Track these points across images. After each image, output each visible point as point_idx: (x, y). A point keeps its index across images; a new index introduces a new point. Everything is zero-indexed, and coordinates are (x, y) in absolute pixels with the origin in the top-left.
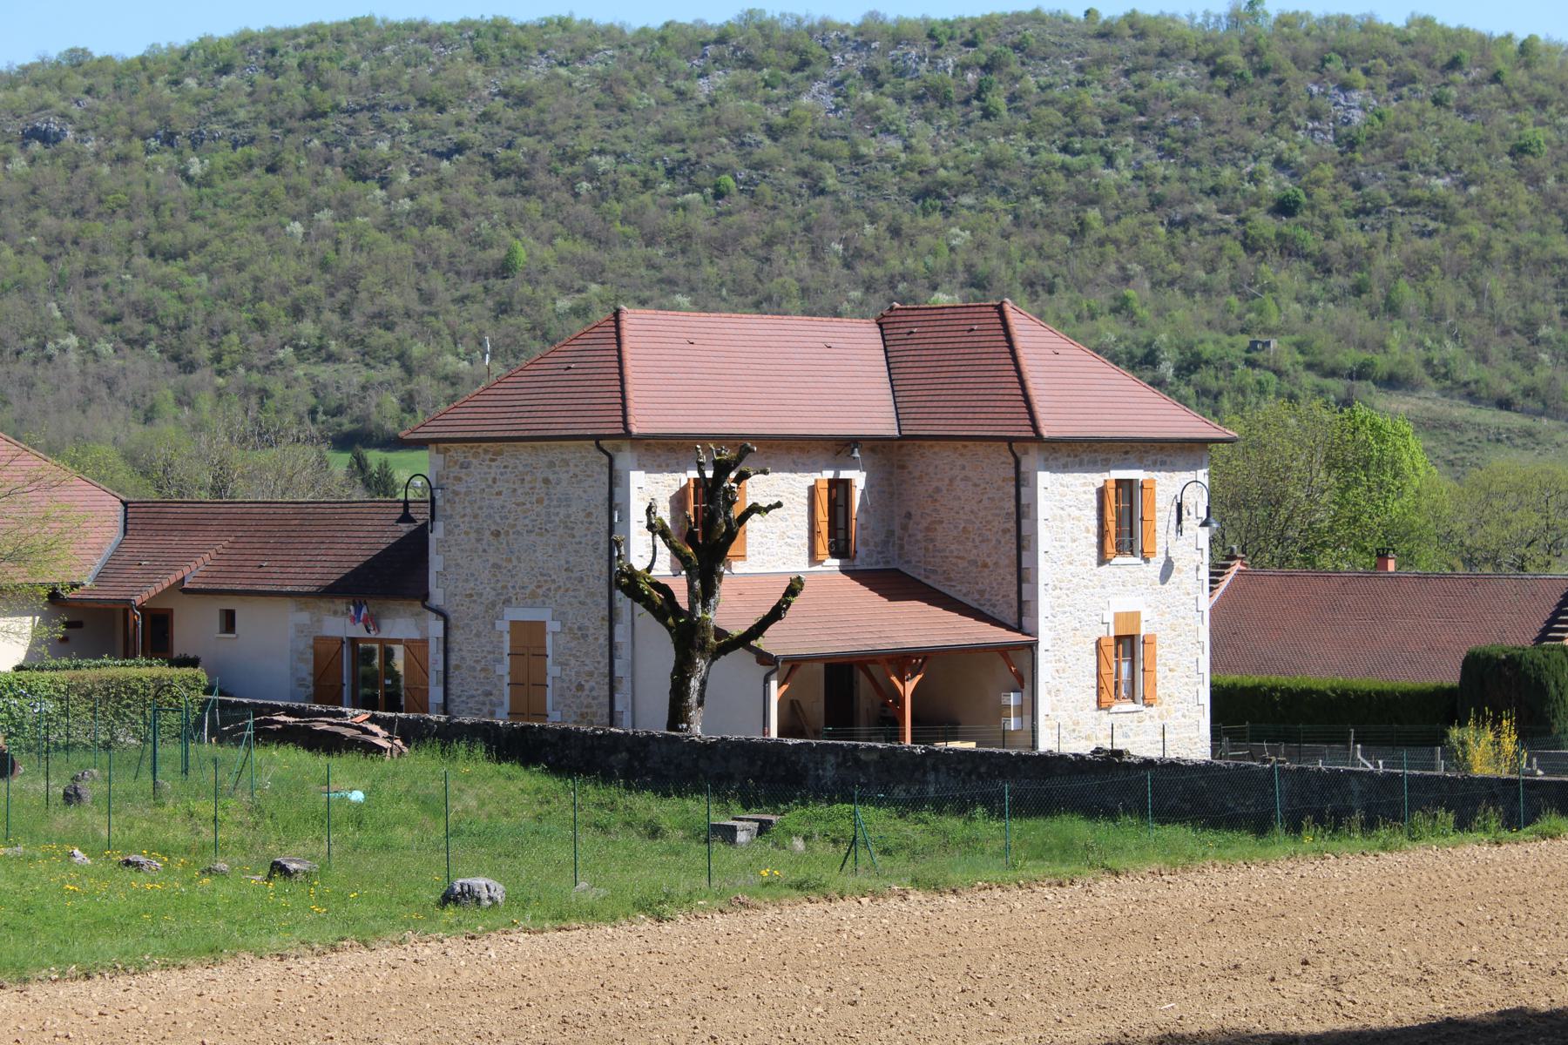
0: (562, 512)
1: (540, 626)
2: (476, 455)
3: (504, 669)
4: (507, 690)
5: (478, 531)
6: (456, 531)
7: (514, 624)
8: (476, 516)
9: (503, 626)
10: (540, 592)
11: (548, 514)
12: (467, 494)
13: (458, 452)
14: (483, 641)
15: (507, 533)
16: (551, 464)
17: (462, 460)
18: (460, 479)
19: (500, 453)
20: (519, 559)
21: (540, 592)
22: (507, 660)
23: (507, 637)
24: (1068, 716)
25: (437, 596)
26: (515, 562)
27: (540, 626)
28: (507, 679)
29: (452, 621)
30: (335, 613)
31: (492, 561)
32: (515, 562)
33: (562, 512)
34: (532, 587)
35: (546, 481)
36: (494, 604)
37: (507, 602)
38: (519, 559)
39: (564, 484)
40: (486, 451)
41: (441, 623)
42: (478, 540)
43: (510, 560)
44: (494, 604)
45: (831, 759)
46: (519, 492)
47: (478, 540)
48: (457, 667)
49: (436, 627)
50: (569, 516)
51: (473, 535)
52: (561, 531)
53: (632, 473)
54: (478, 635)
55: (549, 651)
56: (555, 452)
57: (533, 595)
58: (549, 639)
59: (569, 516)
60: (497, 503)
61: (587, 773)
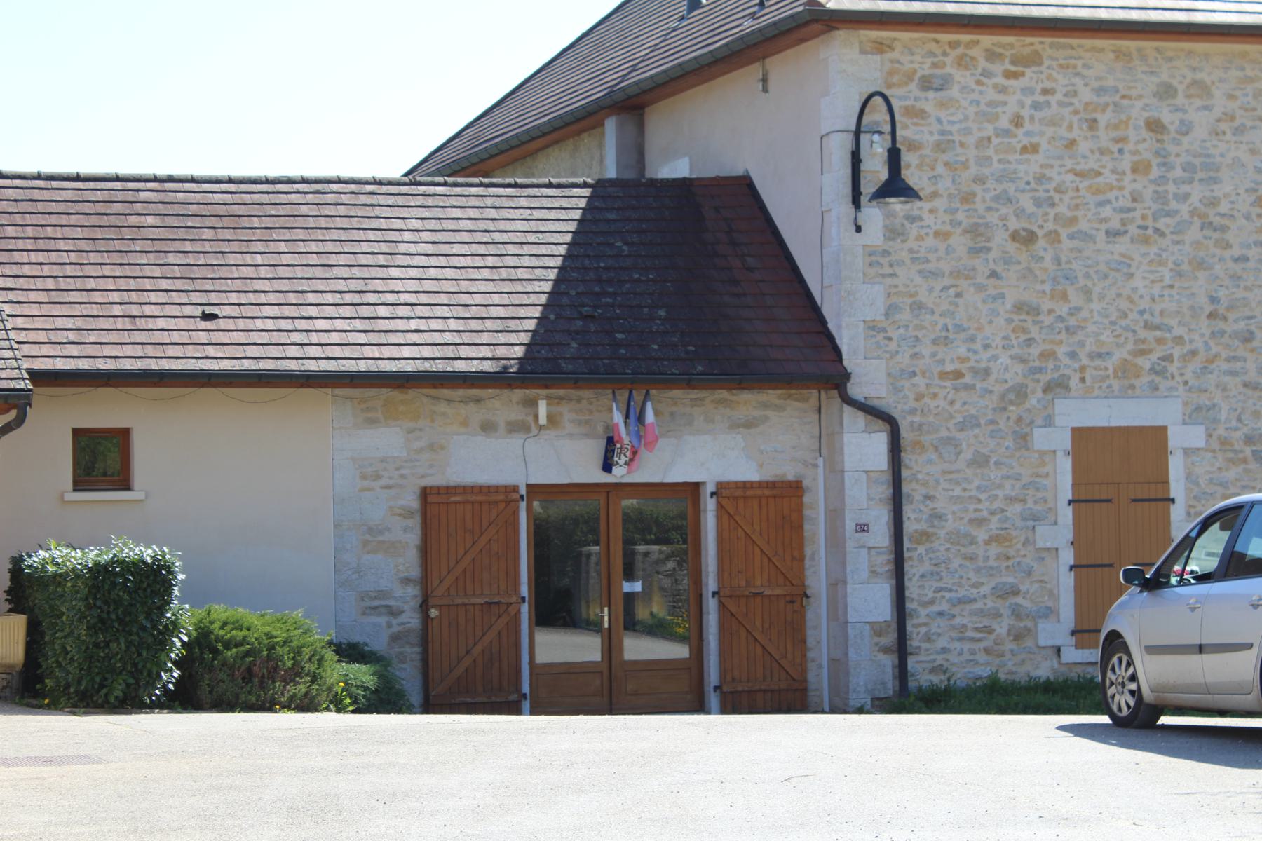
0: (1197, 193)
1: (1157, 436)
2: (961, 62)
3: (1059, 532)
4: (1067, 581)
5: (974, 231)
6: (913, 230)
7: (1081, 435)
8: (968, 198)
9: (1054, 440)
10: (1145, 363)
11: (1160, 197)
12: (940, 147)
13: (913, 50)
14: (994, 474)
15: (1054, 237)
16: (1166, 92)
17: (926, 70)
18: (922, 114)
19: (1034, 60)
20: (1087, 292)
21: (1145, 363)
22: (1066, 515)
23: (1065, 466)
24: (596, 656)
25: (869, 375)
26: (1075, 299)
27: (1157, 436)
28: (1068, 557)
29: (905, 433)
30: (488, 428)
31: (1011, 297)
32: (1075, 299)
33: (1197, 193)
34: (1120, 354)
35: (1155, 126)
36: (1020, 393)
37: (1057, 387)
38: (1087, 292)
39: (1200, 132)
40: (992, 56)
41: (880, 441)
42: (975, 251)
43: (1064, 296)
44: (1020, 393)
45: (680, 651)
46: (1084, 147)
47: (975, 251)
48: (925, 536)
49: (865, 449)
50: (1214, 203)
51: (960, 242)
52: (1193, 233)
53: (599, 659)
54: (980, 461)
55: (1177, 488)
56: (1180, 60)
57: (1126, 370)
58: (1176, 468)
59: (1214, 203)
60: (1033, 165)
61: (934, 692)
